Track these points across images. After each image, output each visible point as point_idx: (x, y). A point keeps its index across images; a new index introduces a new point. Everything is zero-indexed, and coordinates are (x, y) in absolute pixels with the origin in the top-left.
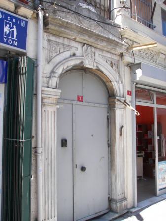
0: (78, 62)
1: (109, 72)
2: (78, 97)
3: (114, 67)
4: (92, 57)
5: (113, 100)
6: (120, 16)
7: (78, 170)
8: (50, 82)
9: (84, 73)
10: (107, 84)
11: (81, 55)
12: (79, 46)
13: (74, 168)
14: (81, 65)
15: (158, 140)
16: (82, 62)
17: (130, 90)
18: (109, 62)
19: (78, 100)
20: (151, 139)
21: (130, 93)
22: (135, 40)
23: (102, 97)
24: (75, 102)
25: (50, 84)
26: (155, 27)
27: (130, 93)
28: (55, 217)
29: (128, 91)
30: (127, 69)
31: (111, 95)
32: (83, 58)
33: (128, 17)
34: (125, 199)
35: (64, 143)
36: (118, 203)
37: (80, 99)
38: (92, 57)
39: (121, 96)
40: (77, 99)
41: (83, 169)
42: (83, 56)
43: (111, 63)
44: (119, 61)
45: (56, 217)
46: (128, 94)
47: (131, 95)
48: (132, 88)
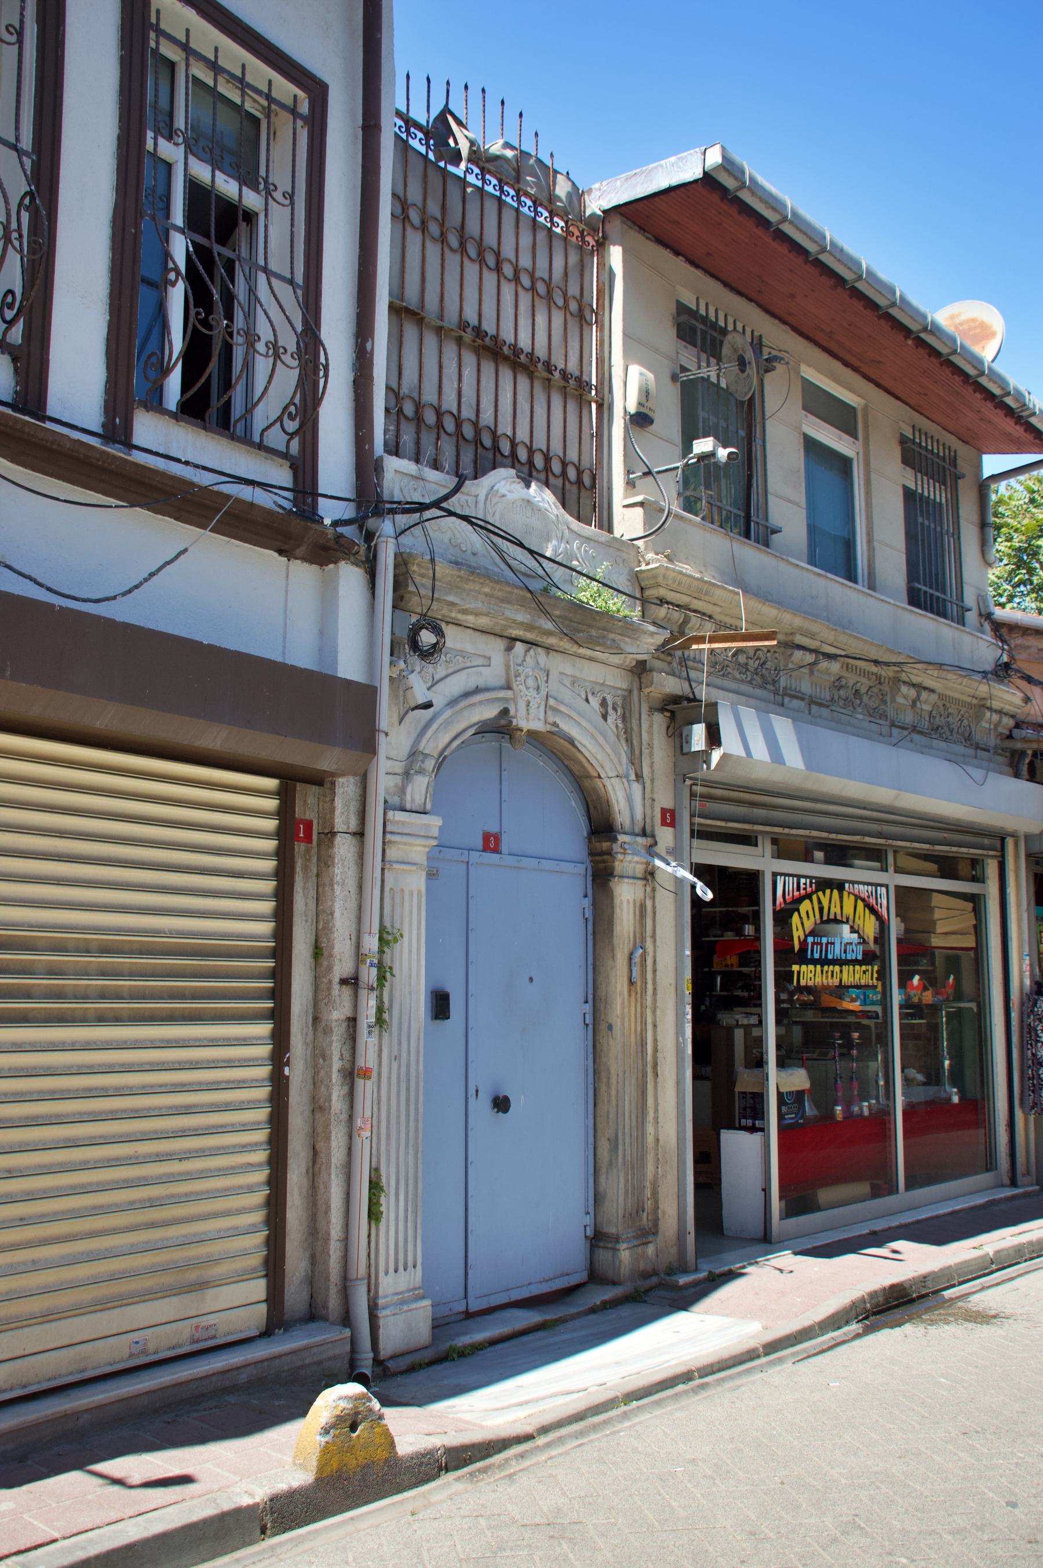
0: (490, 712)
1: (598, 747)
2: (486, 837)
3: (612, 717)
4: (538, 689)
5: (605, 845)
6: (639, 510)
7: (482, 1106)
8: (409, 789)
9: (506, 744)
10: (587, 783)
11: (502, 681)
12: (495, 648)
13: (472, 1100)
14: (503, 722)
15: (828, 861)
16: (505, 712)
17: (669, 804)
18: (595, 702)
19: (486, 848)
20: (762, 1094)
21: (669, 818)
22: (696, 604)
23: (568, 836)
24: (475, 857)
25: (408, 797)
26: (775, 531)
27: (669, 818)
28: (415, 1267)
29: (664, 811)
30: (660, 720)
31: (601, 828)
32: (509, 694)
33: (695, 682)
34: (647, 1233)
35: (440, 1005)
36: (623, 1246)
37: (491, 843)
38: (538, 689)
39: (637, 830)
40: (479, 843)
41: (501, 1104)
42: (509, 687)
43: (604, 703)
44: (630, 691)
45: (419, 1267)
46: (664, 823)
47: (672, 824)
48: (677, 796)
